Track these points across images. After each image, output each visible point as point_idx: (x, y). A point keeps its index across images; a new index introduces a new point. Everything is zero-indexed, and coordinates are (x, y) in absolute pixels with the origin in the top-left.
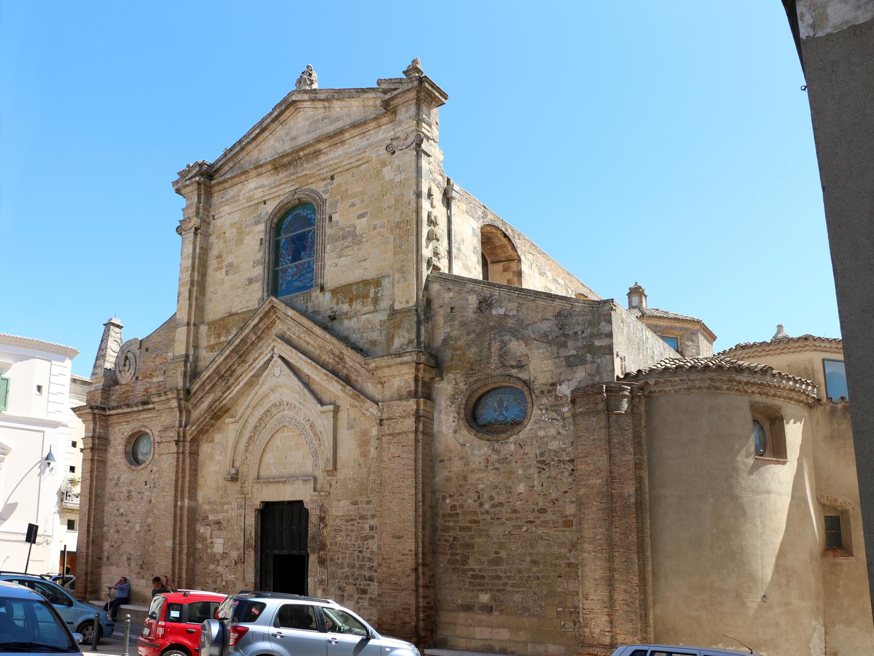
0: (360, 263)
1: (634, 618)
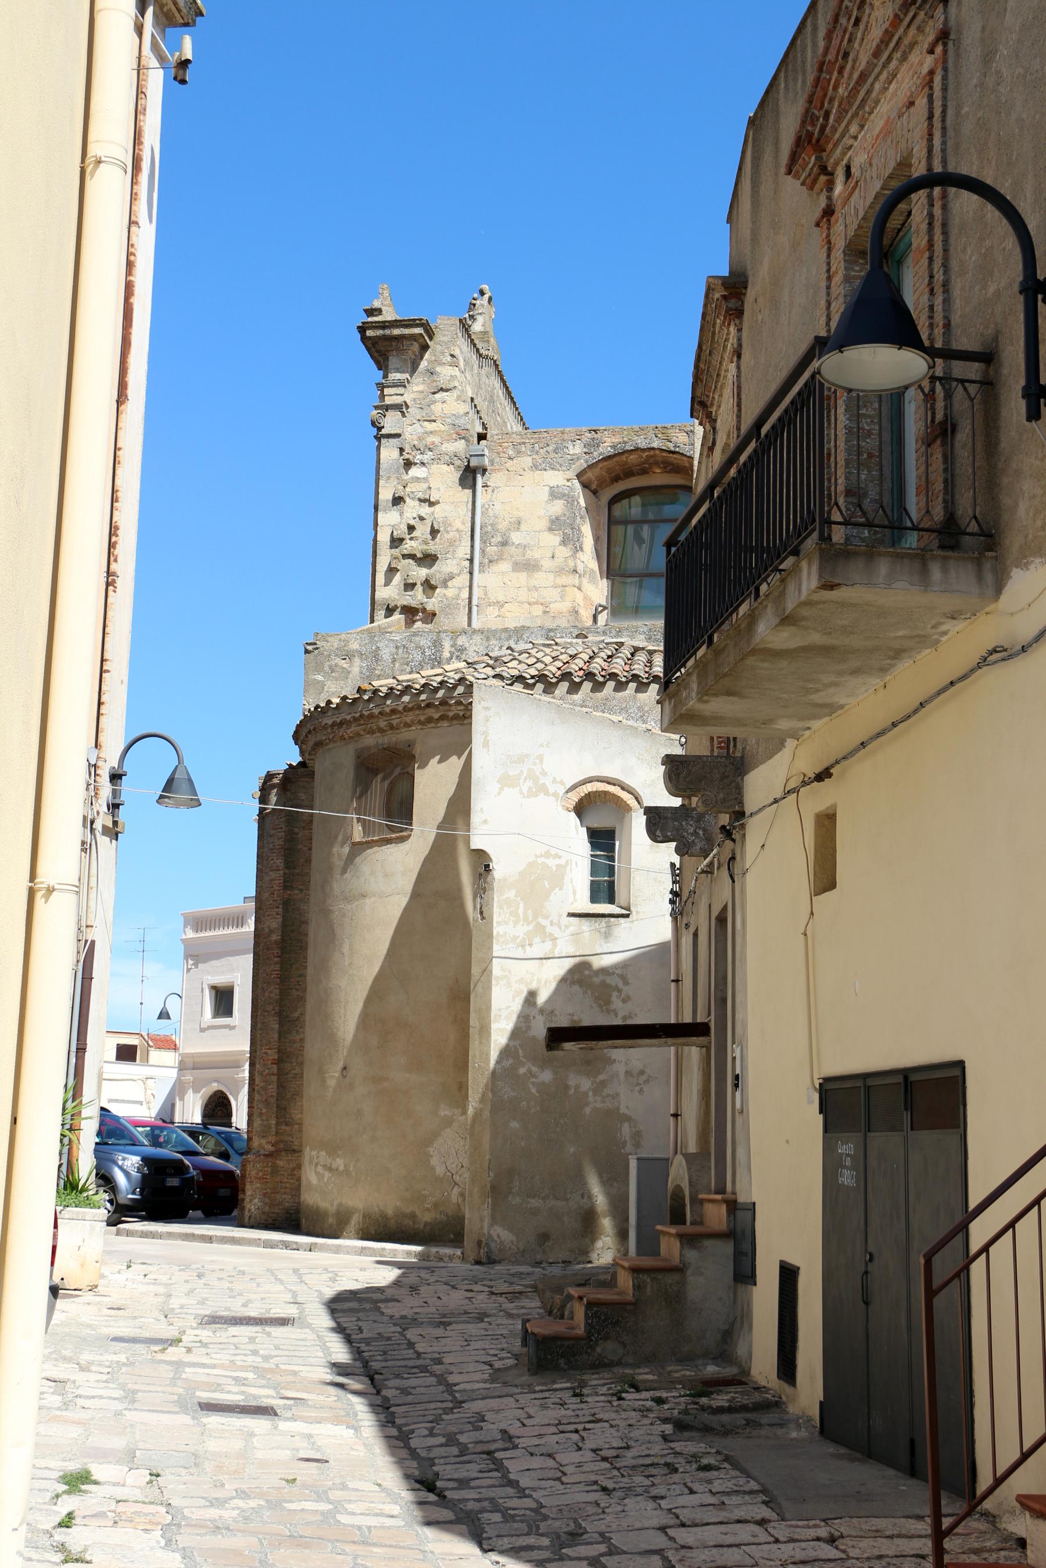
1: (264, 1111)
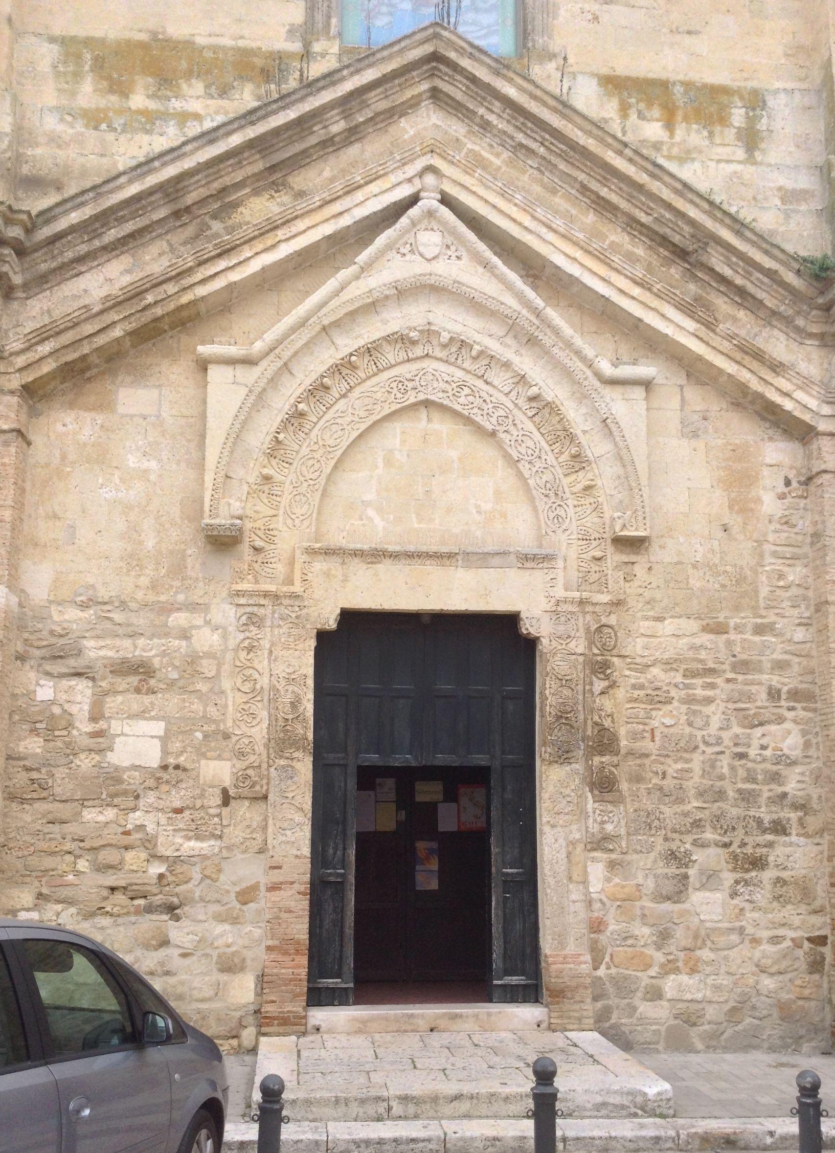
0: (678, 38)
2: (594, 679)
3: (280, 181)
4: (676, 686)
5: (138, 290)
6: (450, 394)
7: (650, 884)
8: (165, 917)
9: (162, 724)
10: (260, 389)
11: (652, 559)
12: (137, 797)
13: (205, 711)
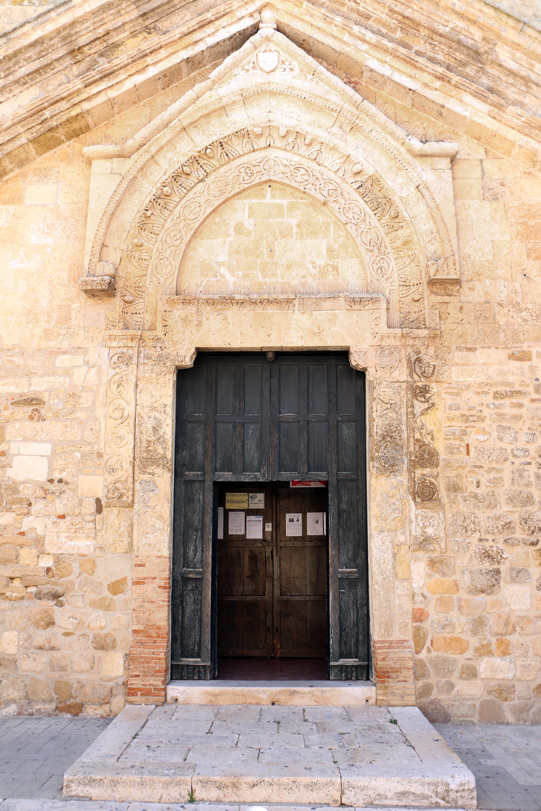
2: (415, 402)
3: (152, 26)
4: (488, 406)
5: (39, 108)
6: (289, 175)
7: (467, 579)
8: (52, 603)
9: (49, 446)
10: (131, 177)
11: (463, 299)
12: (30, 504)
13: (83, 435)
